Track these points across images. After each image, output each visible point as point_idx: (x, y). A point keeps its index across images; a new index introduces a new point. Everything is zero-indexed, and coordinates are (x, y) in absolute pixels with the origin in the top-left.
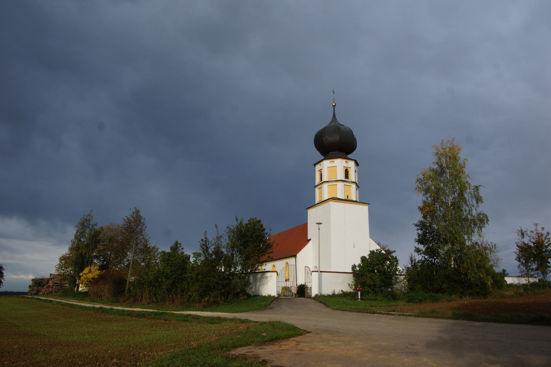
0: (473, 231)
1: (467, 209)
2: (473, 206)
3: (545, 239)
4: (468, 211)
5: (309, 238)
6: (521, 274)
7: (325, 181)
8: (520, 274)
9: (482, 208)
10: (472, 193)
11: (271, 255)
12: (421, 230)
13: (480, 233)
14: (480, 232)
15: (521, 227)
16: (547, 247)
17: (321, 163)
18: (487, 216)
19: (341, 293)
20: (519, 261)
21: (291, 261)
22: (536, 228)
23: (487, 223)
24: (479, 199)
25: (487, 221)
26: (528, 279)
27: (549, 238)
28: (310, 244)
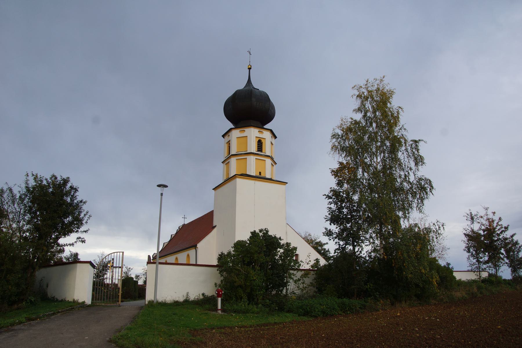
0: (410, 206)
1: (402, 173)
2: (411, 169)
3: (497, 226)
4: (403, 177)
5: (214, 225)
6: (471, 268)
7: (233, 154)
8: (470, 268)
9: (423, 172)
10: (409, 150)
11: (83, 235)
12: (336, 203)
13: (421, 208)
14: (420, 206)
15: (470, 210)
16: (498, 235)
17: (230, 134)
18: (430, 182)
19: (201, 297)
20: (469, 251)
21: (192, 252)
22: (487, 213)
23: (431, 192)
24: (419, 160)
25: (430, 189)
26: (480, 274)
27: (502, 225)
28: (214, 231)
